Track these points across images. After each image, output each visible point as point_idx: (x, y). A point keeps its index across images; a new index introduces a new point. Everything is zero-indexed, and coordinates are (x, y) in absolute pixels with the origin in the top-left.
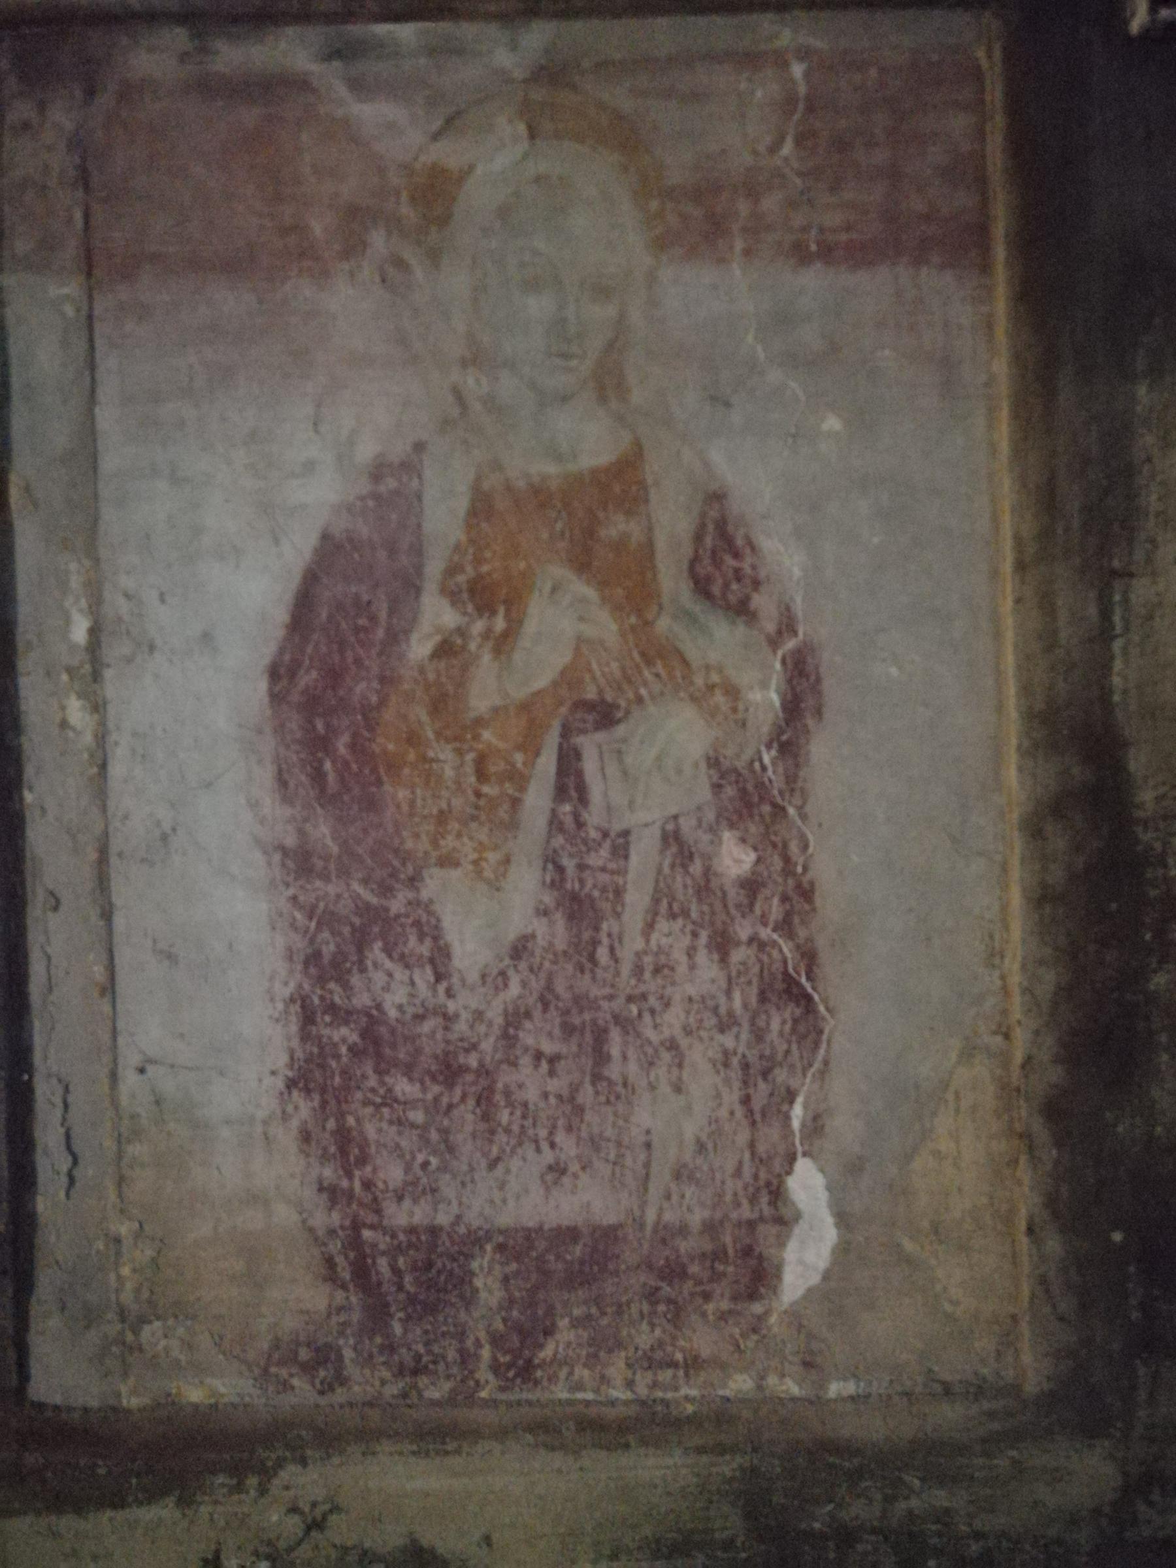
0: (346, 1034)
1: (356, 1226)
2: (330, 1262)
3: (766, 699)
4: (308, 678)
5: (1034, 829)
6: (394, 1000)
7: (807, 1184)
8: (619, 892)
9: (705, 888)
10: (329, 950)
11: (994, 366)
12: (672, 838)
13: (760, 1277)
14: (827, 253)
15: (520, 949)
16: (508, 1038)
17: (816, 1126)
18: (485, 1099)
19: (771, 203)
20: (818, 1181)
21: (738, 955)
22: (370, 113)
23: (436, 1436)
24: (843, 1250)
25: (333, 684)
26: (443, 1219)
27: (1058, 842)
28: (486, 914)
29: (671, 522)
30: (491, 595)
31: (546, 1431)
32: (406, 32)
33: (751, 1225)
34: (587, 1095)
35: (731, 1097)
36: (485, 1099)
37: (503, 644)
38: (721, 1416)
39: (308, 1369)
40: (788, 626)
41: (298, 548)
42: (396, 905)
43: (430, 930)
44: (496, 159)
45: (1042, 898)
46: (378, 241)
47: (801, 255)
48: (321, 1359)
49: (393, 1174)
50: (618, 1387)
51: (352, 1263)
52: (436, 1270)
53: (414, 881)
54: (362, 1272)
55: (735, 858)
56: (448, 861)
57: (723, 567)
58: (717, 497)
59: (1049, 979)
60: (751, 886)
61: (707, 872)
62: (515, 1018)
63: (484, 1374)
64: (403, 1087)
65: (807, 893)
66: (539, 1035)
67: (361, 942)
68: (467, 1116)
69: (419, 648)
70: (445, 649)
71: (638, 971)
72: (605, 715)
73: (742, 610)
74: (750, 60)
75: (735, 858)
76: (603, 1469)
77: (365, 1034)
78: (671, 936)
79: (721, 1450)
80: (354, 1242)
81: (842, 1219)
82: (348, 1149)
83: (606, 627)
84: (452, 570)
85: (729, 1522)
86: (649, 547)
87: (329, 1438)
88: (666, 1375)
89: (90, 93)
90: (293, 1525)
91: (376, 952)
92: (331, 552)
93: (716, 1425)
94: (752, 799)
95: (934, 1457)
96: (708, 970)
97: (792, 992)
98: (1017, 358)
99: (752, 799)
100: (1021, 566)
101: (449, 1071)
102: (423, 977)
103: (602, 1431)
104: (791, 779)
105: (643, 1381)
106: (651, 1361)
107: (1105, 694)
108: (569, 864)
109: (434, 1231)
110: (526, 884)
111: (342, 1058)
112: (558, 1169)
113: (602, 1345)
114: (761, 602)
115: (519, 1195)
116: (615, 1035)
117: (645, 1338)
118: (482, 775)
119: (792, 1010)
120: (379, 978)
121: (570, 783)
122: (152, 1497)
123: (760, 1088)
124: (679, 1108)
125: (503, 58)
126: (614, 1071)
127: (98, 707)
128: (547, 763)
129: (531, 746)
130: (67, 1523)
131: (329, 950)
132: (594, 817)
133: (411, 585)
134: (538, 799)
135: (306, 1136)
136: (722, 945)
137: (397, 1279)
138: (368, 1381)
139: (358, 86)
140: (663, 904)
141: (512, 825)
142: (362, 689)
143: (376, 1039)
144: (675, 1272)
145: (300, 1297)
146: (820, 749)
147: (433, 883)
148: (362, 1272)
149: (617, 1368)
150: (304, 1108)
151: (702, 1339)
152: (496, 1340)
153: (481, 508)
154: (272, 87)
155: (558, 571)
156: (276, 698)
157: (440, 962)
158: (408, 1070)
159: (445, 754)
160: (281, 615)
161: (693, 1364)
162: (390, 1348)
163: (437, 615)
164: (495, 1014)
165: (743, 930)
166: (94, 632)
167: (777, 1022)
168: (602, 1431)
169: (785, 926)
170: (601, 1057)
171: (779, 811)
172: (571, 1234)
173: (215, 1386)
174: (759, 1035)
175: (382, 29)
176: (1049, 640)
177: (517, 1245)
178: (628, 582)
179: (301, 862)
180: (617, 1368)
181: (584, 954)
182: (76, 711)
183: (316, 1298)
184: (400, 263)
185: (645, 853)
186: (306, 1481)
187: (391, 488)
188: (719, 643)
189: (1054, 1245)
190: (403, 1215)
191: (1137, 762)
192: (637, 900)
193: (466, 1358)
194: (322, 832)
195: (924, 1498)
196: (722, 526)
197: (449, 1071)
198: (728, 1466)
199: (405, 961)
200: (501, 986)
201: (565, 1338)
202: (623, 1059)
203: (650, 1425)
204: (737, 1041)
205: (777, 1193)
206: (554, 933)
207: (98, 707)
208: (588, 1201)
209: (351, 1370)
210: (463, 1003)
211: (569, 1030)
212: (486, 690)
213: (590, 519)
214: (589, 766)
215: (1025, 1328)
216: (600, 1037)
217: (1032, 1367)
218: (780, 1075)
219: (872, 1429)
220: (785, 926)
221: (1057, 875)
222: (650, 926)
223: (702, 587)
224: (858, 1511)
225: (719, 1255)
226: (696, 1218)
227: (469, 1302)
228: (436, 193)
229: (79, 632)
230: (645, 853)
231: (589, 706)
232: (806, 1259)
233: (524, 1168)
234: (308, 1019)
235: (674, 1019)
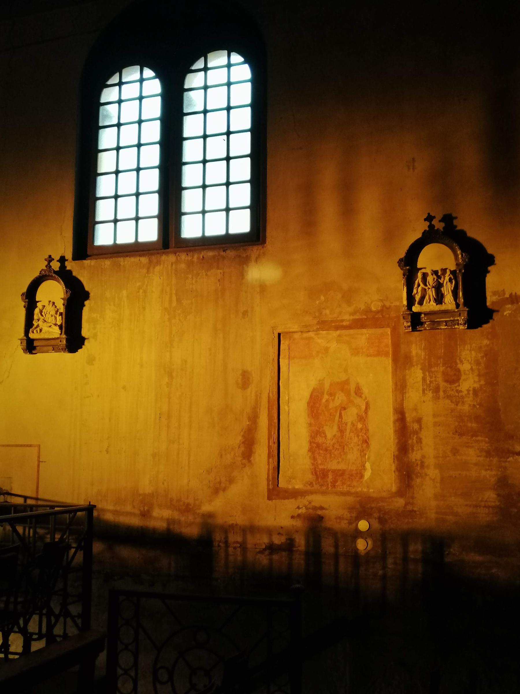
0: (315, 445)
1: (315, 468)
2: (312, 472)
3: (364, 407)
4: (311, 404)
5: (394, 422)
6: (320, 441)
7: (368, 465)
8: (346, 429)
9: (356, 429)
10: (313, 435)
11: (390, 368)
12: (352, 423)
13: (362, 476)
14: (370, 356)
15: (335, 436)
16: (333, 446)
17: (369, 458)
18: (330, 454)
19: (364, 350)
20: (369, 465)
21: (360, 437)
22: (319, 341)
23: (324, 493)
24: (372, 473)
25: (314, 404)
26: (325, 468)
27: (397, 424)
28: (331, 431)
29: (353, 387)
30: (332, 395)
31: (336, 493)
32: (324, 332)
33: (361, 470)
34: (342, 454)
35: (359, 454)
36: (330, 454)
37: (333, 400)
38: (356, 493)
39: (310, 485)
40: (366, 398)
41: (311, 389)
42: (321, 430)
43: (324, 433)
44: (333, 346)
45: (395, 431)
46: (320, 355)
47: (368, 356)
48: (311, 484)
49: (319, 462)
50: (345, 489)
51: (315, 472)
52: (324, 474)
53: (323, 427)
54: (316, 473)
55: (360, 426)
56: (327, 425)
57: (358, 392)
58: (358, 384)
59: (396, 441)
60: (361, 429)
61: (357, 427)
62: (334, 444)
63: (329, 486)
64: (321, 452)
65: (368, 430)
66: (337, 446)
67: (317, 434)
68: (328, 455)
69: (324, 401)
70: (327, 401)
71: (348, 439)
72: (345, 409)
73: (361, 397)
74: (362, 334)
75: (360, 426)
76: (342, 499)
77: (317, 445)
78: (352, 435)
79: (357, 497)
80: (315, 470)
81: (372, 470)
82: (314, 459)
83: (345, 398)
84: (328, 391)
85: (358, 506)
86: (350, 389)
87: (312, 493)
88: (351, 488)
89: (290, 340)
90: (308, 503)
91: (318, 436)
92: (314, 390)
93: (356, 494)
94: (362, 419)
95: (383, 499)
96: (356, 439)
97: (366, 442)
98: (392, 367)
99: (362, 419)
100: (392, 392)
101: (326, 450)
102: (324, 439)
103: (343, 494)
104: (366, 416)
105: (348, 488)
106: (349, 486)
107: (403, 407)
108: (340, 426)
109: (324, 469)
110: (335, 428)
111: (315, 447)
112: (338, 462)
113: (343, 484)
114: (363, 396)
115: (333, 465)
116: (345, 447)
117: (349, 483)
118: (330, 415)
119: (366, 444)
120: (319, 439)
121: (341, 416)
122: (292, 498)
123: (362, 453)
124: (353, 456)
125: (335, 335)
126: (345, 451)
127: (289, 407)
128: (338, 414)
129: (336, 412)
130: (283, 501)
131: (313, 435)
132: (343, 420)
133: (323, 393)
134: (337, 418)
135: (310, 457)
136: (358, 436)
137: (320, 475)
138: (316, 487)
139: (318, 338)
140: (351, 431)
141: (334, 421)
142: (317, 405)
143: (318, 446)
144: (352, 475)
145: (310, 477)
146: (370, 413)
147: (325, 427)
148: (316, 473)
149: (345, 487)
150: (310, 454)
151: (355, 483)
152: (331, 482)
153: (331, 385)
154: (309, 339)
155: (340, 392)
156: (308, 406)
157: (325, 437)
158: (322, 450)
159: (326, 413)
160: (309, 397)
161: (354, 487)
162: (319, 483)
163: (326, 397)
164: (332, 444)
165: (360, 434)
166: (288, 398)
167: (365, 445)
168: (343, 494)
169: (365, 434)
170: (344, 449)
171: (365, 420)
172: (339, 470)
173: (298, 486)
174: (362, 447)
175: (321, 332)
176: (396, 400)
177: (334, 471)
178: (348, 394)
179: (310, 425)
180: (345, 487)
181: (342, 436)
182: (286, 407)
183: (310, 476)
184: (322, 357)
185: (349, 425)
186: (310, 498)
187: (321, 383)
188: (358, 401)
189: (397, 473)
190: (321, 467)
191: (407, 415)
192: (348, 431)
193: (328, 485)
194: (313, 421)
195: (381, 504)
196: (358, 387)
197: (326, 450)
198: (358, 499)
199: (321, 436)
200: (50, 327)
201: (339, 483)
202: (346, 449)
203: (348, 493)
204: (359, 447)
205: (364, 466)
206: (339, 434)
207: (289, 407)
208: (342, 466)
209: (314, 485)
210: (328, 442)
211: (340, 446)
212: (331, 405)
213: (343, 386)
214: (343, 414)
215: (393, 485)
216: (344, 447)
217: (394, 489)
218: (365, 452)
219: (375, 495)
220: (365, 434)
221: (397, 429)
222: (350, 433)
223: (356, 394)
224: (373, 505)
225: (357, 473)
226: (355, 469)
227: (328, 477)
228: (327, 349)
229: (287, 399)
230: (349, 425)
231: (343, 407)
232: (367, 475)
233: (335, 462)
234: (311, 443)
235: (352, 445)
